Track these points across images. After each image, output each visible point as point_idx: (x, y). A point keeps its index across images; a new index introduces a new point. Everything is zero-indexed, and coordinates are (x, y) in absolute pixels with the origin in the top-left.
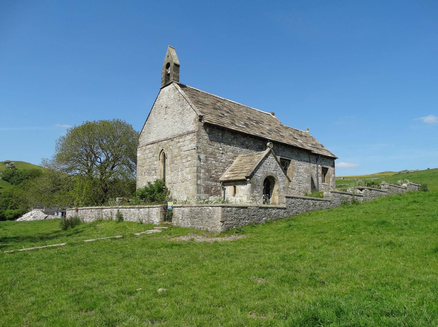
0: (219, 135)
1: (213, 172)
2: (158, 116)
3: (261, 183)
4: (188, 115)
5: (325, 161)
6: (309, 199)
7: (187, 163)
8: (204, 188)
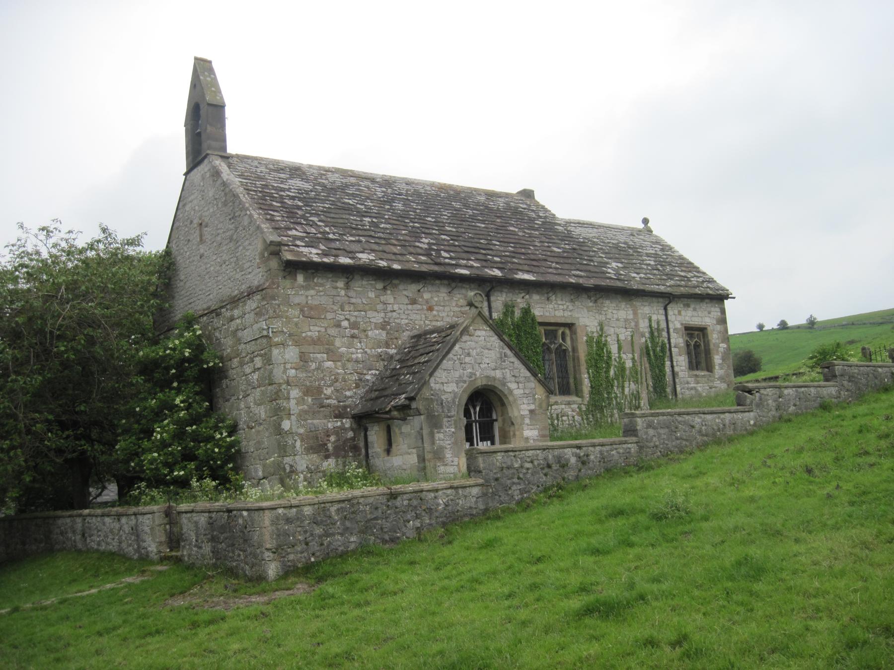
0: (337, 288)
3: (457, 413)
4: (247, 242)
5: (695, 309)
6: (563, 447)
7: (256, 376)
8: (302, 440)
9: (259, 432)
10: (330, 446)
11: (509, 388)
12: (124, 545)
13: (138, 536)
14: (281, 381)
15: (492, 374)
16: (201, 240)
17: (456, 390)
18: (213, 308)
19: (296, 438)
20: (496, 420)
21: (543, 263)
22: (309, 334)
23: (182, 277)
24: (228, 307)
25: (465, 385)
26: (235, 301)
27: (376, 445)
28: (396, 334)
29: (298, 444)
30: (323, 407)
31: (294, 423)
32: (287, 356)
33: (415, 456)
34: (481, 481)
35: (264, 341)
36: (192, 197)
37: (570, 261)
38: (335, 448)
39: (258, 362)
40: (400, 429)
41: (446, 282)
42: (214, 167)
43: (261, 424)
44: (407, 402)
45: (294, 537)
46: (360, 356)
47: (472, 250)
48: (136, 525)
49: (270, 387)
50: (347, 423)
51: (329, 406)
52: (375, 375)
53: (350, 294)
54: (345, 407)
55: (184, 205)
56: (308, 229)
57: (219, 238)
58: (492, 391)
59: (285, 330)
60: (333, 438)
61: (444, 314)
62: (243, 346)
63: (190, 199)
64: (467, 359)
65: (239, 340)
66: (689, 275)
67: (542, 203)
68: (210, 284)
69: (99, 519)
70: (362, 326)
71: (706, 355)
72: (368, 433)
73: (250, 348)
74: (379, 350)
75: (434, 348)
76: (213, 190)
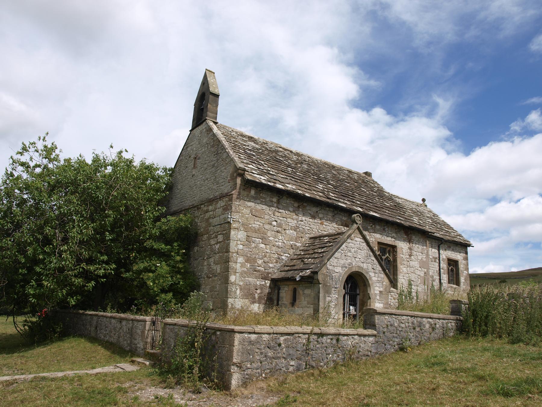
0: (272, 201)
1: (260, 262)
2: (184, 171)
3: (340, 285)
4: (224, 168)
6: (422, 317)
7: (217, 246)
8: (241, 289)
9: (214, 280)
10: (257, 296)
11: (370, 275)
12: (121, 339)
13: (131, 335)
14: (234, 251)
15: (362, 265)
16: (194, 167)
17: (341, 272)
18: (196, 204)
19: (238, 287)
20: (359, 294)
21: (382, 210)
22: (253, 225)
23: (179, 187)
24: (206, 204)
25: (346, 270)
26: (211, 201)
27: (284, 299)
28: (302, 235)
29: (238, 292)
30: (256, 271)
31: (238, 278)
32: (239, 237)
33: (312, 309)
34: (375, 332)
35: (227, 225)
36: (193, 143)
37: (394, 211)
38: (259, 297)
39: (220, 238)
40: (303, 291)
41: (332, 210)
42: (209, 126)
43: (216, 276)
44: (312, 275)
45: (253, 356)
46: (280, 244)
47: (344, 196)
48: (132, 328)
49: (226, 254)
50: (268, 283)
51: (259, 271)
52: (287, 257)
53: (279, 207)
54: (268, 273)
55: (182, 156)
56: (259, 167)
57: (206, 166)
58: (360, 276)
59: (240, 221)
60: (258, 291)
61: (329, 228)
62: (212, 228)
63: (191, 144)
64: (349, 254)
65: (210, 224)
66: (450, 231)
67: (375, 180)
68: (195, 192)
69: (108, 319)
70: (284, 227)
71: (456, 276)
72: (280, 291)
73: (218, 228)
74: (292, 243)
75: (327, 245)
76: (207, 139)
